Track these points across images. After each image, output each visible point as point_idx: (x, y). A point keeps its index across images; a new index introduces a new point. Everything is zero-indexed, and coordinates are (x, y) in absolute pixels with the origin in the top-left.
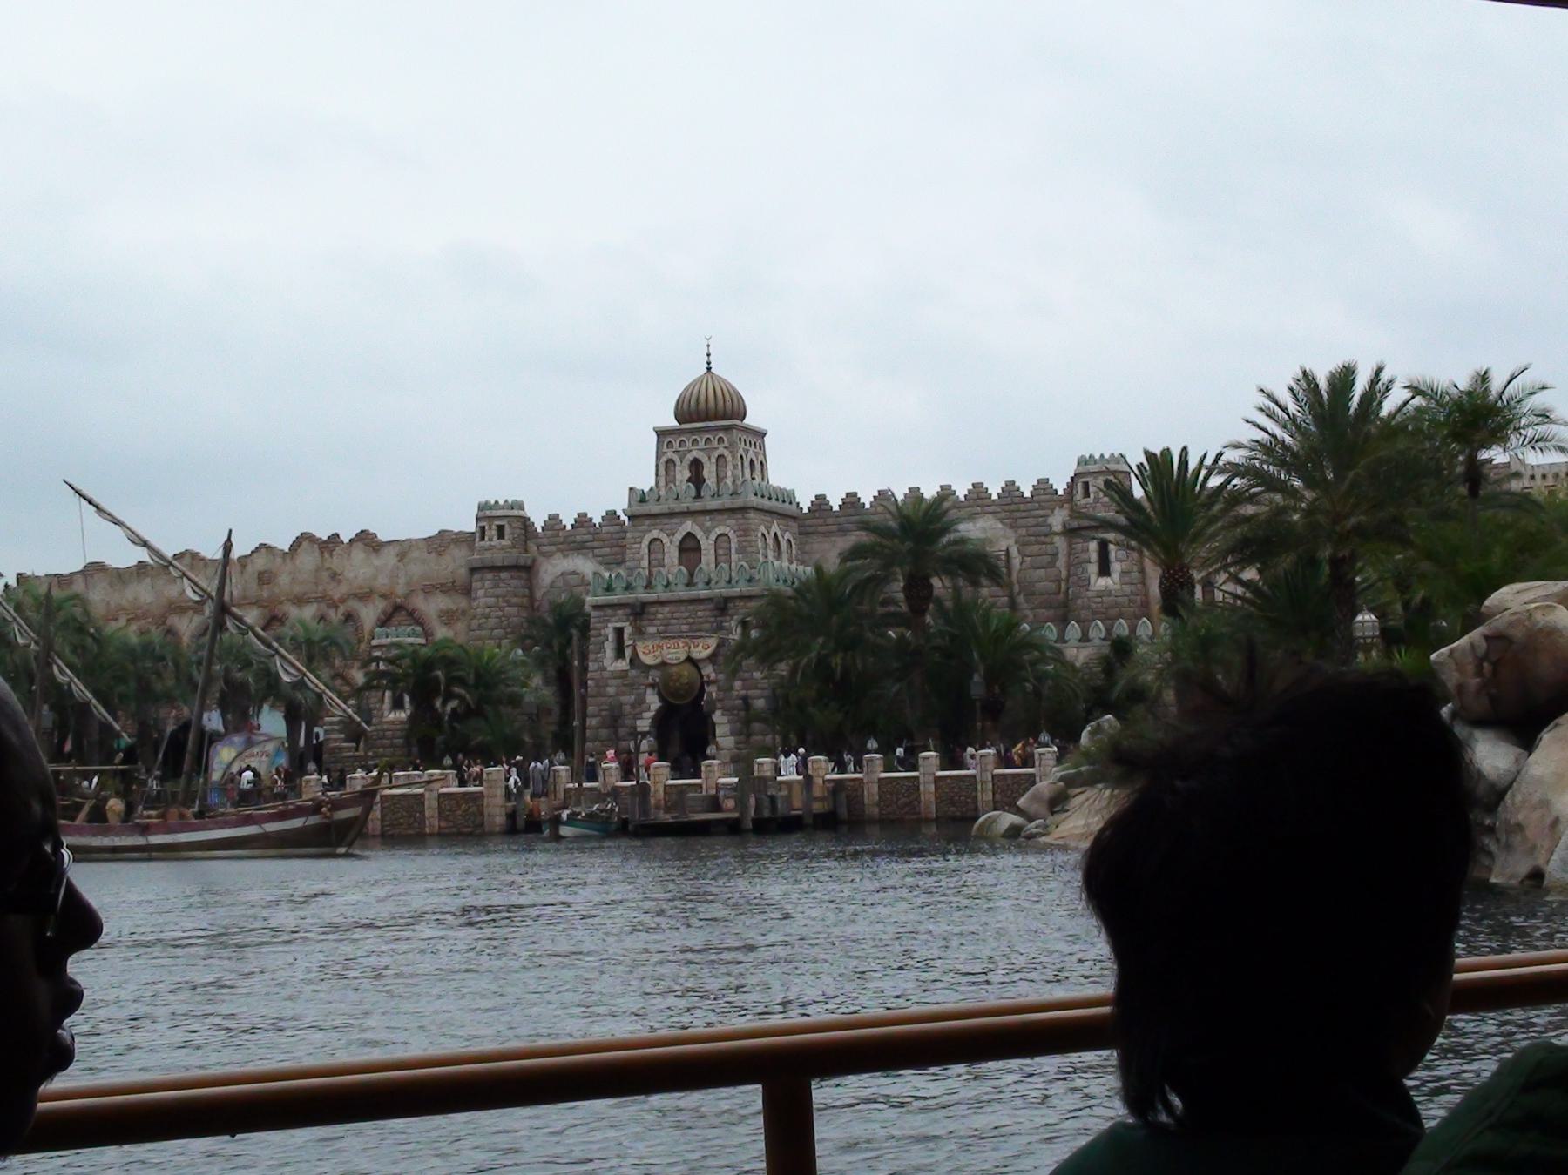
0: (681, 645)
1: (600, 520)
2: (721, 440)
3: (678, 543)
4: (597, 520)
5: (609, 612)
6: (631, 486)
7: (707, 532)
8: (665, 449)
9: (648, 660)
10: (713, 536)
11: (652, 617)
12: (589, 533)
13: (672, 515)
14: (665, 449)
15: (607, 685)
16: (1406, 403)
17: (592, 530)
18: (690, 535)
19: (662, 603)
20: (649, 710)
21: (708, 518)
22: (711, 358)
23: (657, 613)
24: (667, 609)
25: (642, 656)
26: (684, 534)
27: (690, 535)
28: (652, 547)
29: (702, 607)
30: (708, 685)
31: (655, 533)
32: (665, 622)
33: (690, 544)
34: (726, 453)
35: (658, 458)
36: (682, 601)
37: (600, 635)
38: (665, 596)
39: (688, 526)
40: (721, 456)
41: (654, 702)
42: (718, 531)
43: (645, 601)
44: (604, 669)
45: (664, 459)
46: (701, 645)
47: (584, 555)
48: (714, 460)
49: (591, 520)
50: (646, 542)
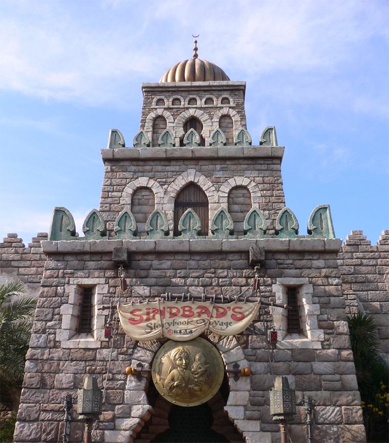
0: (196, 311)
1: (31, 242)
2: (225, 100)
3: (173, 195)
4: (27, 242)
5: (74, 262)
6: (115, 128)
7: (217, 183)
8: (154, 105)
9: (136, 332)
10: (226, 189)
11: (143, 273)
12: (16, 253)
13: (169, 160)
14: (154, 105)
15: (57, 372)
16: (317, 350)
17: (20, 250)
18: (192, 186)
19: (159, 254)
20: (128, 415)
21: (218, 167)
22: (198, 52)
23: (150, 268)
24: (167, 264)
25: (124, 325)
26: (184, 183)
27: (192, 186)
28: (139, 196)
29: (226, 263)
30: (236, 378)
31: (142, 181)
32: (162, 281)
33: (192, 197)
34: (232, 113)
35: (145, 114)
36: (191, 253)
37: (56, 295)
38: (170, 243)
39: (190, 175)
40: (226, 117)
41: (139, 403)
42: (232, 182)
43: (133, 249)
44: (56, 345)
45: (152, 115)
46: (230, 313)
47: (8, 272)
48: (216, 119)
49: (21, 241)
50: (129, 190)
